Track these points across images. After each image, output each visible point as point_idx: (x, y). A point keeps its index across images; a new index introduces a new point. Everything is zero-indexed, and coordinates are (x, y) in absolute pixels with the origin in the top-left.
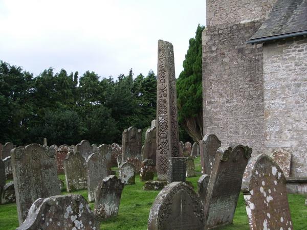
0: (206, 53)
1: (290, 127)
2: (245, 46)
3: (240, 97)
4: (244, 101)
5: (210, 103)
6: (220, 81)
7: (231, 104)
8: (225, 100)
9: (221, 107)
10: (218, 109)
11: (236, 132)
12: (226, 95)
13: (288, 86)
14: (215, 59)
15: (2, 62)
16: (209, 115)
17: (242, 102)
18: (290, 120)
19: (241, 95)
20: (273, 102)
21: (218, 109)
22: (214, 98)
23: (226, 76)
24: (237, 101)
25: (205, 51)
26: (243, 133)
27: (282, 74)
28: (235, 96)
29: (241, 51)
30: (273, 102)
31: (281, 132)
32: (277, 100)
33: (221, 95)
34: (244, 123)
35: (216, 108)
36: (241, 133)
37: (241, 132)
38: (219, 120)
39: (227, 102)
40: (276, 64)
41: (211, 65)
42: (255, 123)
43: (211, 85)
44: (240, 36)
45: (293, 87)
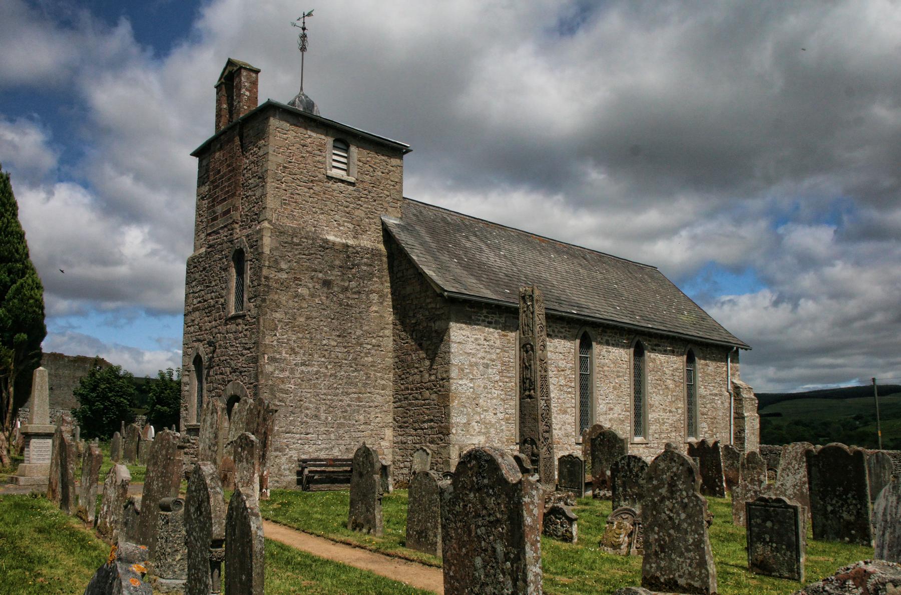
0: (269, 267)
1: (478, 418)
2: (333, 278)
3: (323, 359)
4: (329, 367)
5: (273, 360)
6: (291, 324)
7: (310, 369)
8: (299, 359)
9: (292, 371)
10: (287, 373)
11: (317, 417)
12: (302, 351)
13: (476, 364)
14: (284, 286)
15: (874, 380)
16: (270, 382)
17: (327, 367)
18: (478, 409)
19: (324, 356)
20: (460, 382)
21: (287, 373)
22: (280, 353)
23: (302, 319)
24: (319, 365)
25: (267, 263)
26: (327, 418)
27: (470, 347)
28: (316, 356)
29: (327, 284)
30: (460, 382)
31: (469, 423)
33: (293, 349)
34: (328, 402)
35: (283, 370)
36: (323, 418)
37: (323, 416)
38: (286, 392)
39: (303, 364)
40: (464, 333)
41: (276, 293)
42: (344, 403)
43: (276, 329)
44: (326, 258)
45: (481, 368)
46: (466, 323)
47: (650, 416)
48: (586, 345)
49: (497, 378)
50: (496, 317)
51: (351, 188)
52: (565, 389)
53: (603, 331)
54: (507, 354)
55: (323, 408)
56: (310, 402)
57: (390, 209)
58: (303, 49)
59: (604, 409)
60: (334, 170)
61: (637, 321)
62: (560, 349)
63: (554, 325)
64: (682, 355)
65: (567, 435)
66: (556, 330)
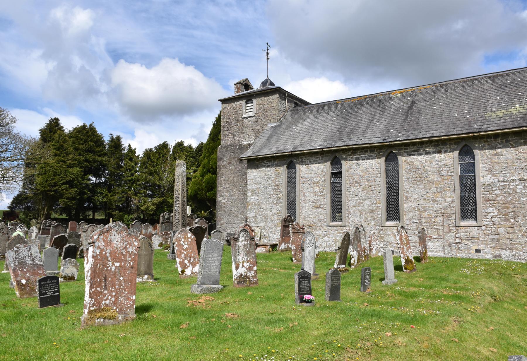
5: (221, 196)
8: (230, 194)
32: (254, 197)
33: (228, 190)
35: (225, 199)
46: (255, 169)
47: (405, 206)
48: (291, 166)
49: (272, 193)
50: (272, 163)
51: (254, 118)
52: (319, 194)
53: (352, 153)
54: (278, 180)
55: (240, 212)
56: (235, 211)
57: (272, 120)
58: (268, 59)
59: (354, 203)
60: (247, 114)
61: (457, 131)
62: (315, 170)
63: (311, 158)
64: (283, 165)
65: (320, 220)
66: (312, 160)
